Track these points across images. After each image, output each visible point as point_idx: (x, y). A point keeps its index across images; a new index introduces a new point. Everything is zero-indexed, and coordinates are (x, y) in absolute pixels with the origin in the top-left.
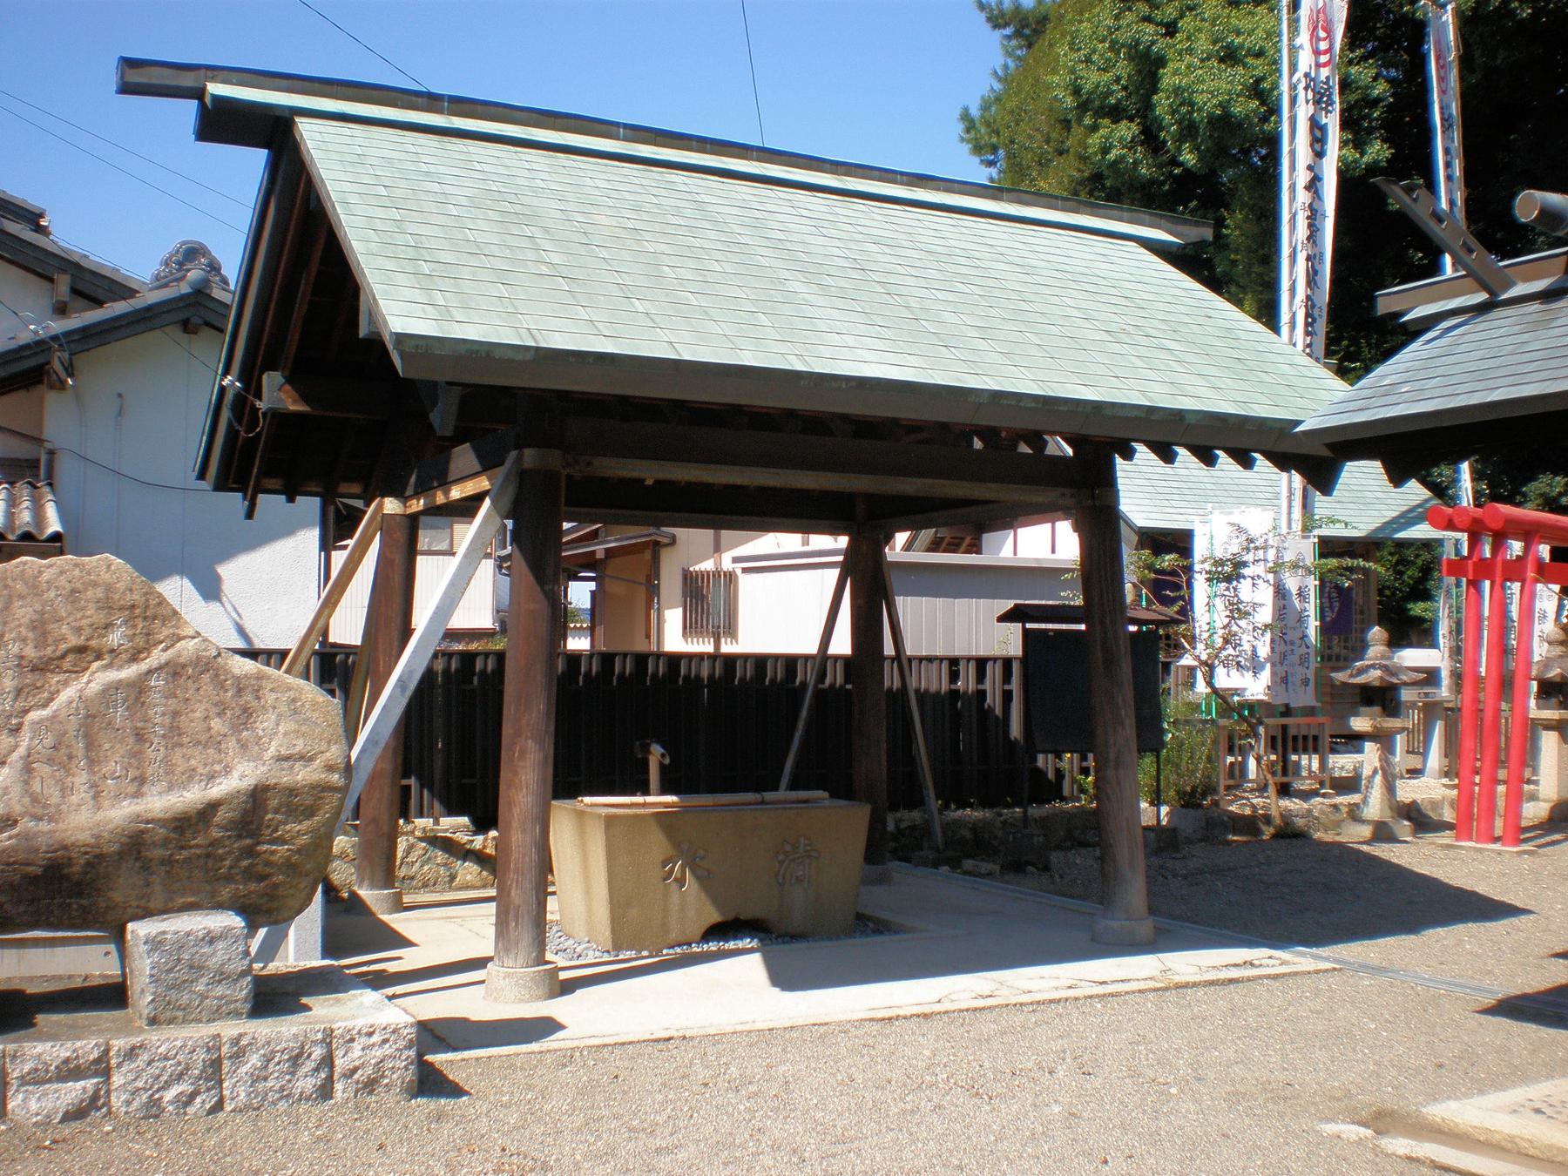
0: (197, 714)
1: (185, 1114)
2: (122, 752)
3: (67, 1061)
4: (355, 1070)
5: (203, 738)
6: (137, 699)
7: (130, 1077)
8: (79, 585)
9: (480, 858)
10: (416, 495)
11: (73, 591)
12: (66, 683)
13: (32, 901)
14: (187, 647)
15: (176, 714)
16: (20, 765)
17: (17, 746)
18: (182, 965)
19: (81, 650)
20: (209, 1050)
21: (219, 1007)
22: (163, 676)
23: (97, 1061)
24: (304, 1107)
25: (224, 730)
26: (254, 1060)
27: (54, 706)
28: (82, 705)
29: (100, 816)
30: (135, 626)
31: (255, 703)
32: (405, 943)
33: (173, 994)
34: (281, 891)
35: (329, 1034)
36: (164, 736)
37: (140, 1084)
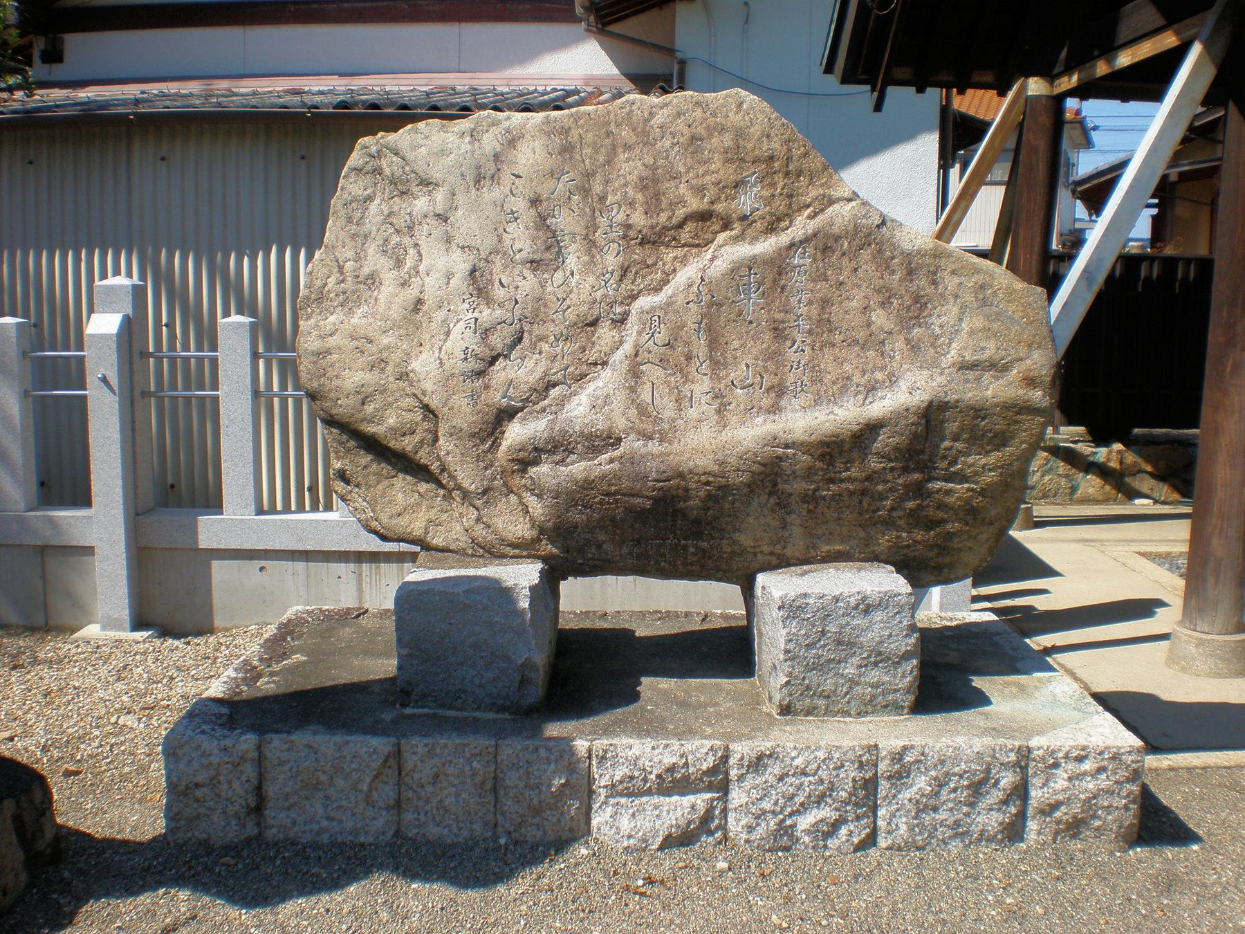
0: (854, 304)
1: (825, 847)
2: (755, 351)
3: (671, 769)
4: (1055, 806)
5: (861, 335)
6: (775, 281)
7: (755, 795)
8: (701, 130)
9: (1102, 471)
10: (1068, 71)
11: (693, 138)
12: (684, 261)
13: (638, 542)
14: (841, 214)
15: (825, 303)
16: (625, 367)
17: (621, 342)
18: (827, 637)
19: (704, 217)
20: (861, 765)
21: (874, 697)
22: (810, 250)
23: (712, 771)
24: (984, 850)
25: (888, 325)
26: (921, 783)
27: (668, 290)
28: (704, 290)
29: (726, 435)
30: (773, 185)
31: (930, 290)
32: (1046, 571)
33: (813, 678)
34: (955, 543)
35: (1025, 754)
36: (810, 332)
37: (767, 805)
